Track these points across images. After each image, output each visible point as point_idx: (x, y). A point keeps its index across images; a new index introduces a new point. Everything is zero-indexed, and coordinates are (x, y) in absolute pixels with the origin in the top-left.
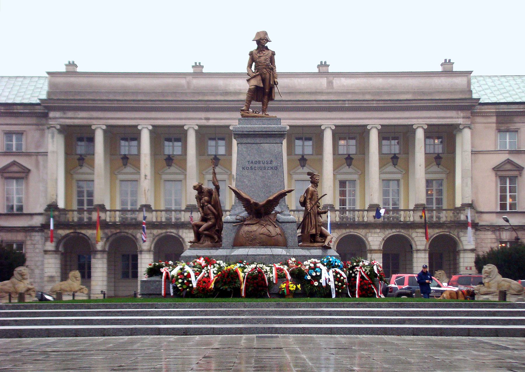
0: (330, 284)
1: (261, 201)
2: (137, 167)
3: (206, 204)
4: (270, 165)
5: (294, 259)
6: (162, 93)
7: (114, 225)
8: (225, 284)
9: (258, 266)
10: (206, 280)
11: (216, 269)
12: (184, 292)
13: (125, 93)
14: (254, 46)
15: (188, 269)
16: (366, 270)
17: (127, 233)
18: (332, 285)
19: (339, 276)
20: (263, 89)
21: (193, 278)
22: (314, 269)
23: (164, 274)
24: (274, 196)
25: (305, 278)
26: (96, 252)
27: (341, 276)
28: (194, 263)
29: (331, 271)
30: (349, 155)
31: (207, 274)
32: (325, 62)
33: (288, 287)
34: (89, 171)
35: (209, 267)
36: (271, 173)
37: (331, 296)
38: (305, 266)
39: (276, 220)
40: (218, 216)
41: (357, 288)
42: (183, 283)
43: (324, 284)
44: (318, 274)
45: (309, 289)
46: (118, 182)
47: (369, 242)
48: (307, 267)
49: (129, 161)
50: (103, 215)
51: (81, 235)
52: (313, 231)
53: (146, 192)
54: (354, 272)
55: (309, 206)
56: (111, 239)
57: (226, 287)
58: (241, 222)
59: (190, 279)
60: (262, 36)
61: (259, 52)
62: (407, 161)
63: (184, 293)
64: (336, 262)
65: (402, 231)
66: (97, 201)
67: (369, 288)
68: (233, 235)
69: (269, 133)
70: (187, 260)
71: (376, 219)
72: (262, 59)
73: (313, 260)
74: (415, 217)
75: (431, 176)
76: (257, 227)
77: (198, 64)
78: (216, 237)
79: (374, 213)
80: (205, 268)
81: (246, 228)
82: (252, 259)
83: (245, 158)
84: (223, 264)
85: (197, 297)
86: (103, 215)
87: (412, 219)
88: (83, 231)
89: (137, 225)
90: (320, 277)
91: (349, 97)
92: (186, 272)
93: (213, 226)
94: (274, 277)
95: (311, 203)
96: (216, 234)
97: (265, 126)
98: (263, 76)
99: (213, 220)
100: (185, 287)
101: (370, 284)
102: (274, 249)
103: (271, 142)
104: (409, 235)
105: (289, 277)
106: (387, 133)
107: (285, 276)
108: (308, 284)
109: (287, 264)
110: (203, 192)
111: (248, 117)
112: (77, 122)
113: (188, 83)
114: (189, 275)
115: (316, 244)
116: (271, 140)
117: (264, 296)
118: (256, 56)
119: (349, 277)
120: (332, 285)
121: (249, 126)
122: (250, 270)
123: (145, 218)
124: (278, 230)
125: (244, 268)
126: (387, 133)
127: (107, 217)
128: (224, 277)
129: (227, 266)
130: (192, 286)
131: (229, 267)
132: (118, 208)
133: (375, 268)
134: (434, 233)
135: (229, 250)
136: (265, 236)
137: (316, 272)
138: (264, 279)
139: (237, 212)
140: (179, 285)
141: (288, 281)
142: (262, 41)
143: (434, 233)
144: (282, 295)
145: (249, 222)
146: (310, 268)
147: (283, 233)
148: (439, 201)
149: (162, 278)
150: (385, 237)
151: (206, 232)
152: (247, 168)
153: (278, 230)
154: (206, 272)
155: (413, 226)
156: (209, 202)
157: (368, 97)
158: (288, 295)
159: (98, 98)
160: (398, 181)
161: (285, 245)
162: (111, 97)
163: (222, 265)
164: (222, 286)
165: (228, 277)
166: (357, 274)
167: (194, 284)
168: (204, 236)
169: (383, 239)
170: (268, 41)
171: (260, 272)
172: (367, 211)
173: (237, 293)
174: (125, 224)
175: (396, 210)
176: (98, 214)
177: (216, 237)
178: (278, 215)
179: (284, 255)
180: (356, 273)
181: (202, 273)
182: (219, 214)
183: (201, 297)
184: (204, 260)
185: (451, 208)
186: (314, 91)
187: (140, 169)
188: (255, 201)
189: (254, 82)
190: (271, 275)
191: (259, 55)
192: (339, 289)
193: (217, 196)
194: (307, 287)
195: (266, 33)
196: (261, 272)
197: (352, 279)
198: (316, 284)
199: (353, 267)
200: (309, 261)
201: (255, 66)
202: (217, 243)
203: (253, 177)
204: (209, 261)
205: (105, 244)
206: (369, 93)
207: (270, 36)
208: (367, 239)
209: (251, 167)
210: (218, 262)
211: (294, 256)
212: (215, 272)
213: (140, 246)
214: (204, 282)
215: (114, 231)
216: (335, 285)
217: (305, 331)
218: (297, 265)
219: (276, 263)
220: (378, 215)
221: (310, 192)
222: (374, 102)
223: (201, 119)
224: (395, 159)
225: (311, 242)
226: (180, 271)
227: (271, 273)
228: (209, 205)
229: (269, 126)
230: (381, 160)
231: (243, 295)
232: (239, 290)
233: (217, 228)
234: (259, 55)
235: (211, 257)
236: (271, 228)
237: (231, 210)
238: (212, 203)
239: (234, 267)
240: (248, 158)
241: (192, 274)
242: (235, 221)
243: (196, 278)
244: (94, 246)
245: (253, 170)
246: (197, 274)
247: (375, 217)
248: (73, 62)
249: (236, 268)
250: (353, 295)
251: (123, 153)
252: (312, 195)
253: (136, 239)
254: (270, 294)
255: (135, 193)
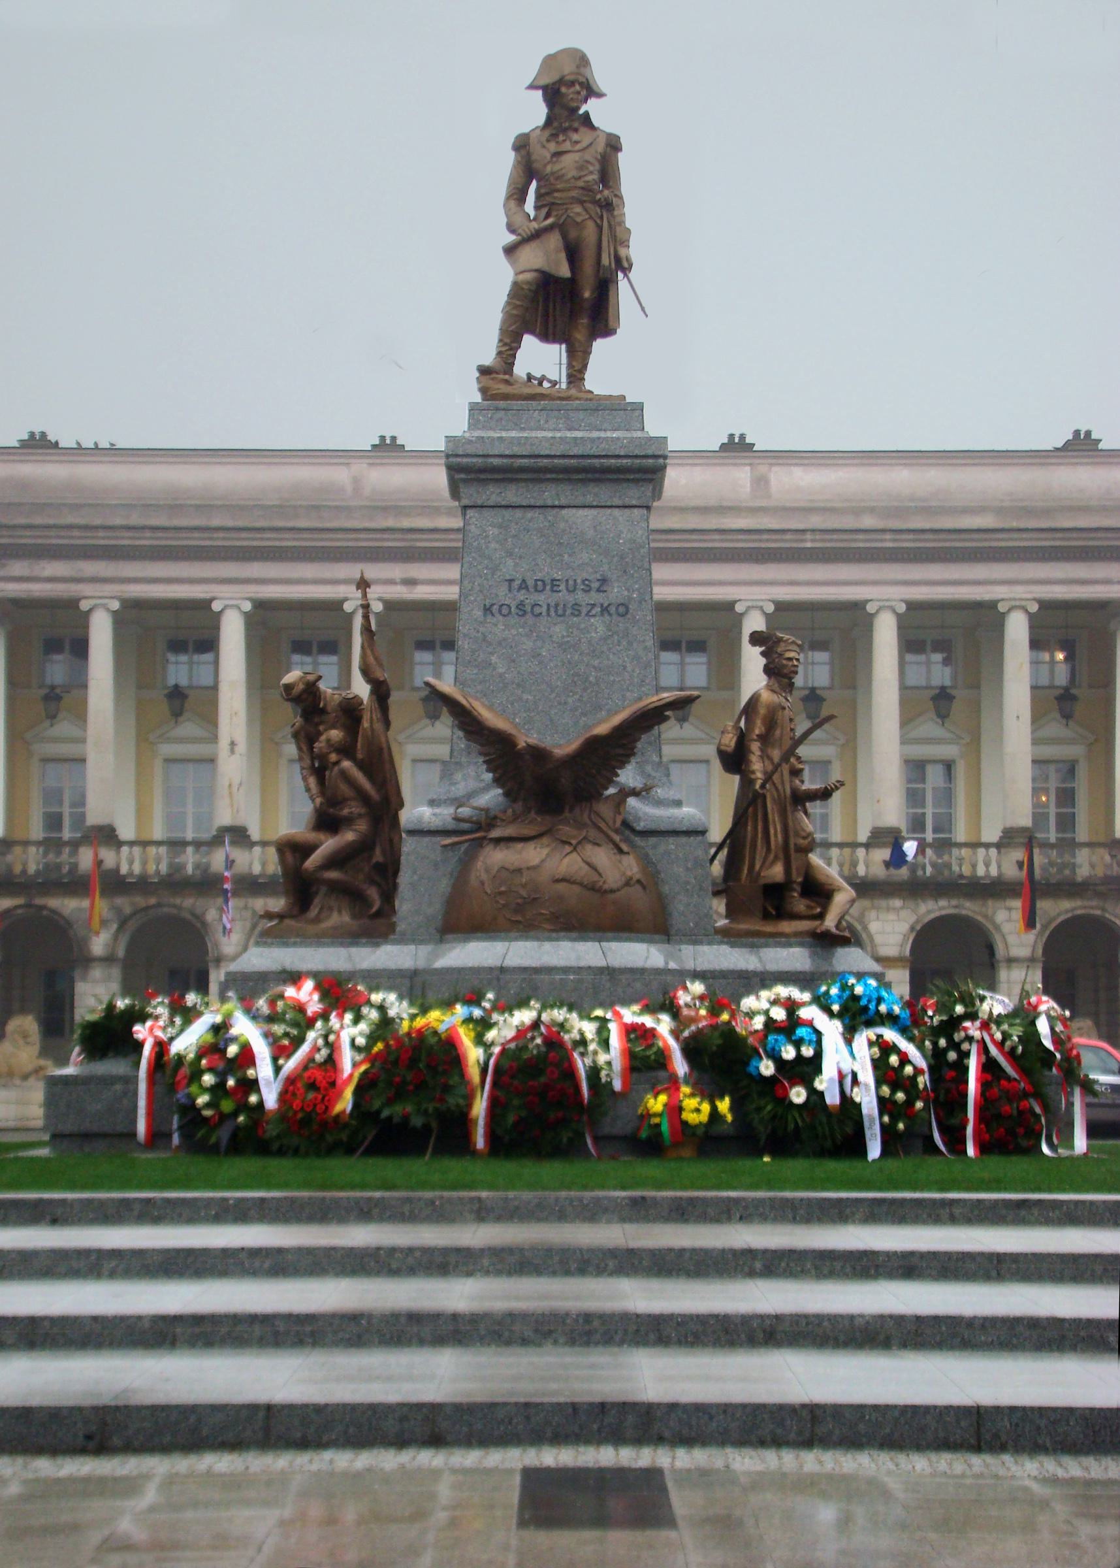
0: (857, 1095)
1: (563, 743)
2: (210, 716)
3: (333, 757)
4: (594, 597)
5: (698, 988)
6: (281, 509)
7: (142, 885)
8: (399, 1093)
9: (545, 1017)
10: (318, 1078)
11: (363, 1026)
12: (222, 1134)
13: (175, 508)
14: (533, 112)
15: (245, 1028)
16: (1006, 1036)
17: (179, 908)
18: (867, 1099)
19: (894, 1060)
20: (571, 287)
21: (263, 1070)
22: (790, 1027)
23: (147, 1050)
24: (617, 720)
25: (751, 1069)
26: (87, 961)
27: (905, 1059)
28: (272, 1003)
29: (862, 1039)
30: (813, 690)
31: (324, 1052)
32: (742, 437)
33: (675, 1109)
34: (74, 732)
35: (334, 1021)
36: (601, 629)
37: (862, 1151)
38: (751, 1015)
39: (625, 824)
40: (384, 808)
41: (971, 1114)
42: (219, 1090)
43: (833, 1099)
44: (808, 1051)
45: (771, 1124)
46: (158, 765)
47: (870, 936)
48: (758, 1023)
49: (188, 704)
50: (108, 856)
51: (45, 913)
52: (776, 872)
53: (235, 789)
54: (956, 1046)
55: (757, 766)
56: (132, 925)
57: (401, 1119)
58: (475, 832)
59: (251, 1072)
60: (568, 69)
61: (554, 136)
62: (975, 707)
63: (223, 1134)
64: (880, 1000)
65: (968, 904)
66: (95, 816)
67: (1021, 1113)
68: (444, 886)
69: (596, 462)
70: (248, 987)
71: (892, 871)
72: (568, 162)
73: (783, 991)
74: (989, 865)
75: (1048, 751)
76: (545, 851)
77: (388, 441)
78: (373, 893)
79: (885, 854)
80: (319, 1024)
81: (496, 857)
82: (518, 987)
83: (494, 570)
84: (398, 1007)
85: (281, 1152)
86: (108, 856)
87: (994, 871)
88: (54, 903)
89: (208, 884)
90: (815, 1064)
91: (816, 521)
92: (234, 1039)
93: (362, 848)
94: (617, 1066)
95: (765, 756)
96: (372, 882)
97: (579, 434)
98: (573, 234)
99: (362, 826)
100: (227, 1106)
101: (1026, 1095)
102: (614, 945)
103: (604, 499)
104: (986, 916)
105: (680, 1066)
106: (925, 630)
107: (662, 1060)
108: (761, 1094)
109: (673, 1010)
110: (323, 711)
111: (505, 397)
112: (37, 589)
113: (357, 481)
114: (247, 1056)
115: (787, 926)
116: (603, 492)
117: (570, 1150)
118: (542, 154)
119: (937, 1059)
120: (867, 1099)
121: (513, 434)
122: (510, 1033)
123: (230, 863)
124: (631, 866)
125: (484, 1024)
126: (925, 630)
127: (128, 862)
128: (396, 1062)
129: (413, 1017)
130: (261, 1104)
131: (420, 1022)
132: (158, 833)
133: (1043, 1026)
134: (1054, 910)
135: (424, 951)
136: (576, 889)
137: (798, 1044)
138: (570, 1073)
139: (460, 789)
140: (202, 1100)
141: (673, 1084)
142: (566, 92)
143: (1054, 910)
144: (647, 1144)
145: (509, 831)
146: (771, 1025)
147: (650, 880)
148: (1066, 822)
149: (137, 1064)
150: (917, 922)
151: (333, 875)
152: (504, 610)
153: (631, 866)
154: (320, 1042)
155: (995, 889)
156: (347, 750)
157: (868, 522)
158: (676, 1144)
159: (98, 522)
160: (949, 766)
161: (657, 925)
162: (135, 519)
163: (392, 1013)
164: (384, 1105)
165: (413, 1062)
166: (967, 1054)
167: (270, 1097)
168: (323, 890)
169: (912, 929)
170: (591, 91)
171: (554, 1042)
172: (867, 846)
173: (452, 1134)
174: (175, 883)
175: (944, 845)
176: (96, 855)
177: (373, 893)
178: (632, 801)
179: (657, 972)
180: (965, 1046)
181: (305, 1049)
182: (386, 800)
183: (296, 1152)
184: (317, 987)
185: (1102, 839)
186: (713, 502)
187: (216, 725)
188: (531, 741)
189: (533, 258)
190: (602, 1058)
191: (553, 147)
192: (894, 1120)
193: (379, 726)
194: (759, 1110)
195: (582, 60)
196: (561, 1044)
197: (949, 1074)
198: (798, 1095)
199: (953, 1023)
200: (764, 994)
201: (539, 196)
202: (376, 923)
203: (528, 644)
204: (338, 993)
205: (116, 937)
206: (872, 510)
207: (600, 76)
208: (865, 928)
209: (521, 605)
210: (376, 998)
211: (697, 975)
212: (361, 1041)
213: (216, 945)
214: (312, 1086)
215: (140, 901)
216: (881, 1100)
217: (820, 1430)
218: (714, 1012)
219: (627, 1002)
220: (898, 857)
221: (762, 711)
222: (888, 536)
223: (391, 582)
224: (942, 699)
225: (766, 916)
226: (209, 1038)
227: (600, 1042)
228: (346, 764)
229: (595, 434)
230: (904, 703)
231: (480, 1142)
232: (463, 1120)
233: (378, 856)
234: (553, 147)
235: (352, 975)
236: (602, 857)
237: (434, 786)
238: (360, 756)
239: (447, 1020)
240: (508, 568)
241: (262, 1050)
242: (451, 825)
243: (277, 1069)
244: (84, 943)
245: (530, 619)
246: (280, 1052)
247: (887, 864)
248: (43, 434)
249: (453, 1028)
250: (956, 1143)
251: (171, 682)
252: (771, 722)
253: (204, 924)
254: (596, 1139)
255: (207, 794)
